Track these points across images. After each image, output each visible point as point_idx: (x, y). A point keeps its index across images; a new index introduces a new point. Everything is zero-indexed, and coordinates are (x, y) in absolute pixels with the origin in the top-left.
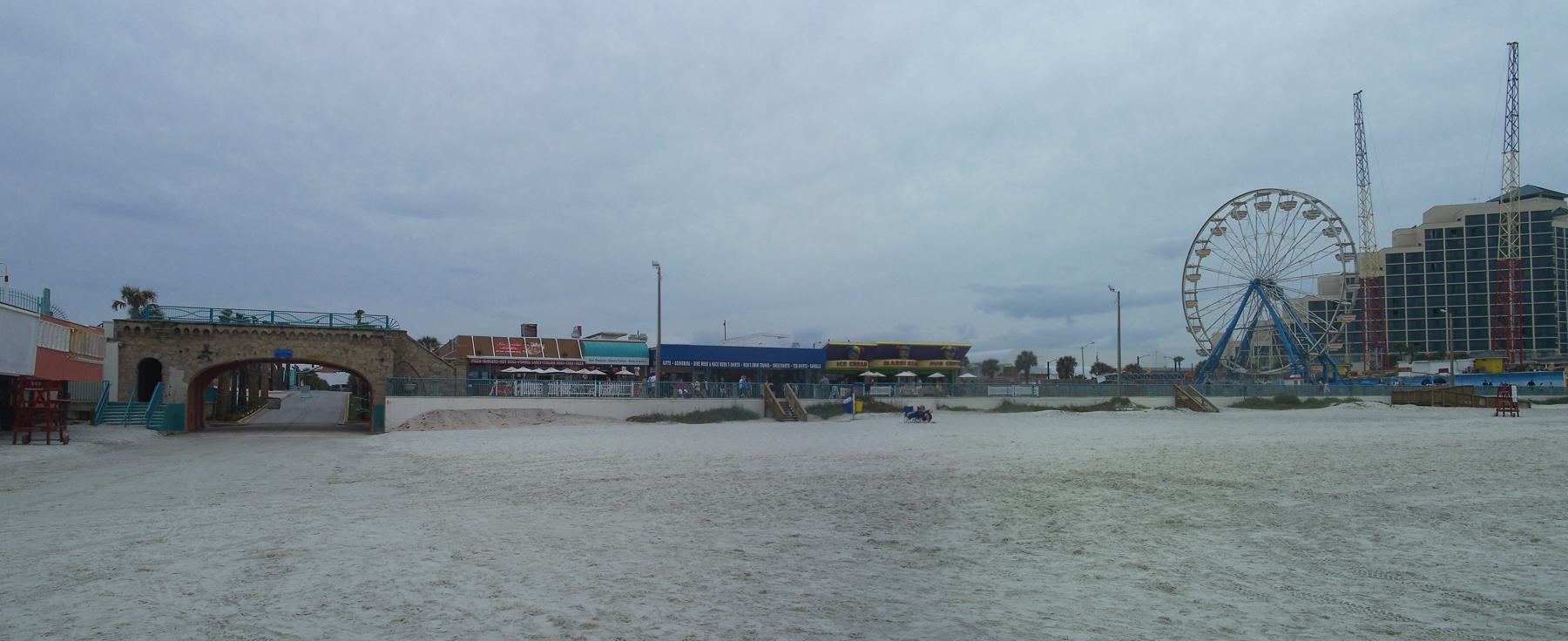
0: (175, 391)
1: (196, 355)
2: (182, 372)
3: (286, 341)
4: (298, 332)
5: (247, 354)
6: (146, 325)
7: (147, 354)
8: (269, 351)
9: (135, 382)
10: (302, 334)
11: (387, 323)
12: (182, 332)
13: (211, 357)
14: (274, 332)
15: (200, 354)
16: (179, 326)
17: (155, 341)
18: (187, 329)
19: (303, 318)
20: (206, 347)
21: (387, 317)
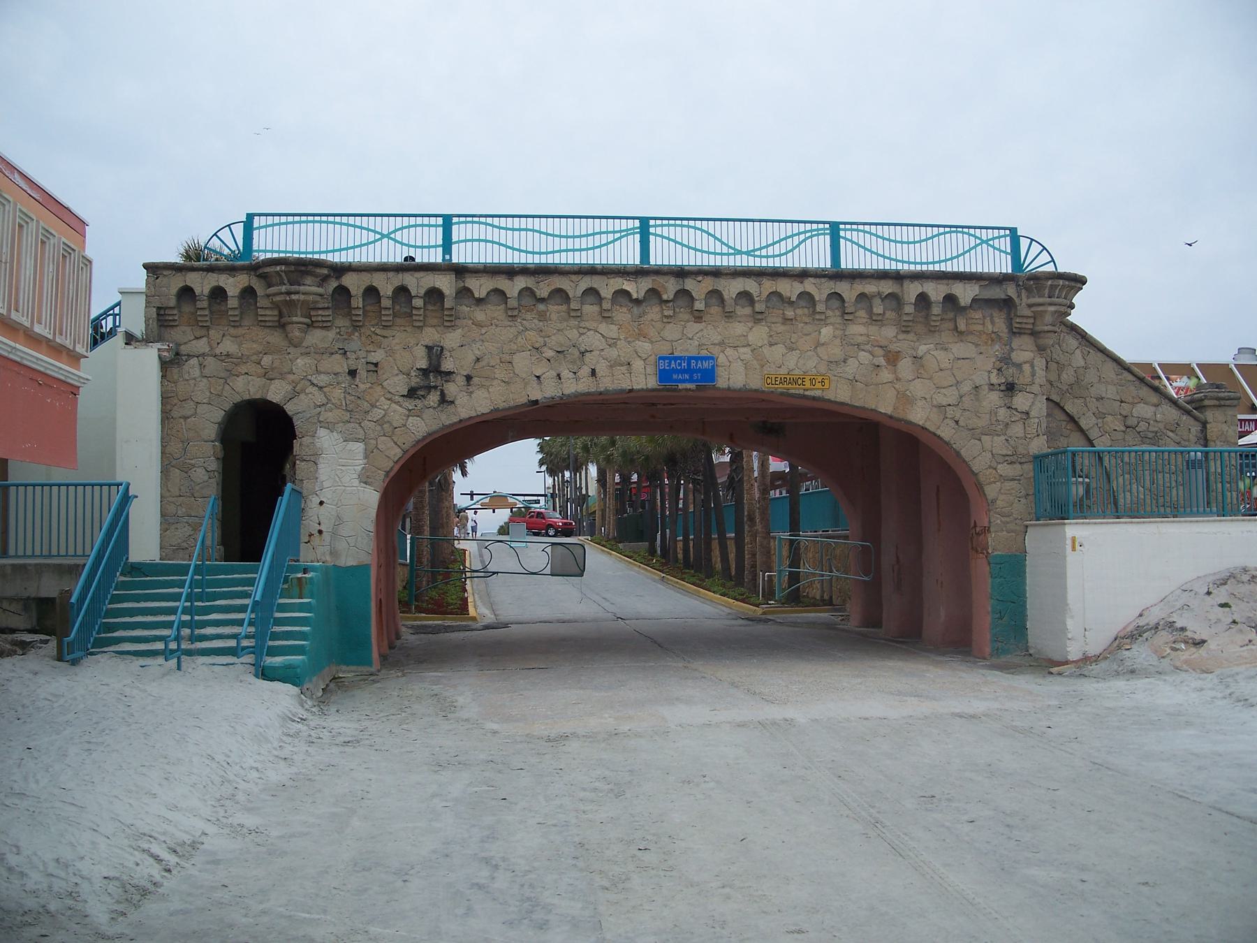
0: (339, 520)
1: (399, 385)
2: (359, 447)
3: (693, 327)
4: (731, 288)
5: (566, 374)
6: (243, 280)
7: (247, 387)
8: (638, 364)
9: (212, 490)
10: (745, 296)
11: (249, 394)
12: (357, 302)
13: (451, 389)
14: (653, 293)
15: (415, 381)
16: (349, 280)
17: (275, 338)
18: (371, 292)
19: (745, 237)
20: (435, 351)
21: (1013, 231)
